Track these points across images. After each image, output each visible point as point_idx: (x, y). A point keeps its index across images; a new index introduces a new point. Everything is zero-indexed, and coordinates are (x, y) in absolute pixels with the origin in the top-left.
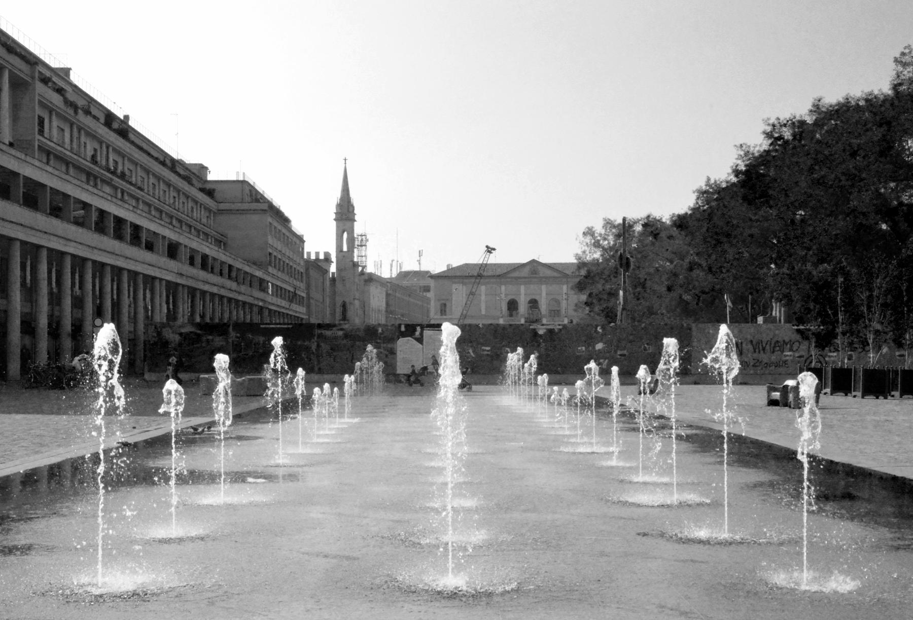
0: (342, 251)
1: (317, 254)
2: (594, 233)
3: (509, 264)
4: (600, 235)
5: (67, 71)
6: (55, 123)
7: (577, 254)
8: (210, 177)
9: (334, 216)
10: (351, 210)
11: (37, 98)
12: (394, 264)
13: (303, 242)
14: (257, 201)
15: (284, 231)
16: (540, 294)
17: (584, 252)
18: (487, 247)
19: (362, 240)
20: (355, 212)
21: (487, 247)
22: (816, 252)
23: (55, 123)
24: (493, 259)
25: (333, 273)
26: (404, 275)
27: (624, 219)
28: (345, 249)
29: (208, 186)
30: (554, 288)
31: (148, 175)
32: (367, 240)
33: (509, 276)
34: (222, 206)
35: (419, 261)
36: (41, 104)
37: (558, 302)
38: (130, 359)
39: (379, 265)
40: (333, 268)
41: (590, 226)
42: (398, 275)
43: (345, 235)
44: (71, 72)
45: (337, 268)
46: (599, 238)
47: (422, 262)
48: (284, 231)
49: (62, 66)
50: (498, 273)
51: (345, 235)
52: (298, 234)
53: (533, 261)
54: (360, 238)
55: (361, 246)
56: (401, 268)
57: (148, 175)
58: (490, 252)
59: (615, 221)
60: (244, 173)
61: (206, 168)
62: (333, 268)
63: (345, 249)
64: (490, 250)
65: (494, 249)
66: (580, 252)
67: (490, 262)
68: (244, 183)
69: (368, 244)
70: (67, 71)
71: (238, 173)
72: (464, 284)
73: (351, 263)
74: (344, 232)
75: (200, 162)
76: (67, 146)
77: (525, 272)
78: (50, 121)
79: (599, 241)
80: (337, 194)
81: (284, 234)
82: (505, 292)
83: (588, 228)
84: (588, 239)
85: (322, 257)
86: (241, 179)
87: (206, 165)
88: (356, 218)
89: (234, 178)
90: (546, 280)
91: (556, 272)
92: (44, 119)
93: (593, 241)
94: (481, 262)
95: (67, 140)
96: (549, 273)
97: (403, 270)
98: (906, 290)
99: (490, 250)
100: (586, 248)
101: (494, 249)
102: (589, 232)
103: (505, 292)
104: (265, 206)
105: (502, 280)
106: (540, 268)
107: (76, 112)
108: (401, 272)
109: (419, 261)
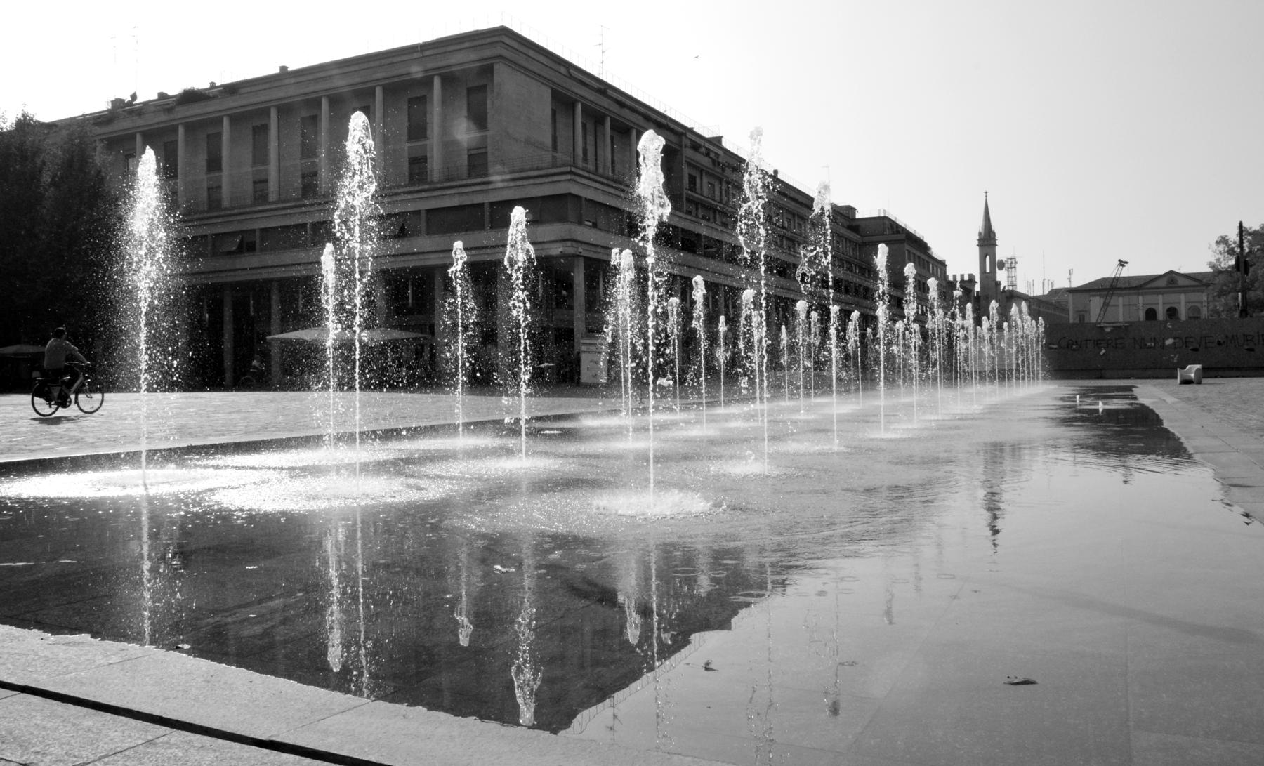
0: (985, 272)
1: (962, 276)
2: (1227, 241)
3: (1146, 276)
4: (1234, 242)
5: (719, 139)
6: (705, 180)
7: (1210, 263)
8: (858, 216)
9: (977, 242)
10: (992, 236)
11: (684, 159)
12: (1046, 282)
13: (945, 266)
14: (898, 232)
15: (923, 256)
16: (1179, 303)
17: (1218, 260)
18: (1120, 261)
19: (1012, 263)
20: (996, 238)
21: (1120, 261)
22: (447, 348)
23: (705, 180)
24: (1126, 272)
25: (978, 292)
26: (1055, 292)
27: (1242, 230)
28: (988, 270)
29: (854, 224)
30: (1194, 297)
31: (794, 217)
32: (1016, 263)
33: (1149, 286)
34: (866, 239)
35: (1070, 279)
36: (689, 164)
37: (1198, 310)
38: (361, 471)
39: (1031, 284)
40: (977, 288)
41: (1223, 234)
42: (1050, 292)
43: (988, 258)
44: (723, 139)
45: (981, 288)
46: (1233, 246)
47: (1072, 280)
48: (923, 256)
49: (715, 135)
50: (1134, 285)
51: (988, 258)
52: (940, 259)
53: (1171, 272)
54: (1010, 261)
55: (1011, 268)
56: (1052, 286)
57: (794, 217)
58: (1123, 266)
59: (1251, 228)
60: (884, 211)
61: (854, 209)
62: (977, 288)
63: (988, 270)
64: (1122, 264)
65: (1127, 263)
66: (1213, 260)
67: (1122, 275)
68: (885, 218)
69: (1017, 266)
70: (719, 139)
71: (879, 210)
72: (1100, 296)
73: (994, 284)
74: (986, 256)
75: (847, 204)
76: (717, 198)
77: (1162, 283)
78: (701, 179)
79: (1233, 248)
80: (979, 224)
81: (924, 260)
82: (1142, 302)
83: (1221, 237)
84: (1222, 247)
85: (966, 278)
86: (882, 215)
87: (853, 206)
88: (998, 243)
89: (877, 215)
90: (1184, 289)
91: (1197, 282)
92: (695, 177)
93: (1226, 249)
94: (1113, 276)
95: (717, 193)
96: (1187, 282)
97: (1055, 288)
98: (503, 566)
99: (1122, 264)
100: (1220, 256)
101: (1127, 263)
102: (1223, 240)
103: (1142, 302)
104: (903, 236)
105: (1140, 291)
106: (1176, 277)
107: (723, 170)
108: (1052, 290)
109: (1070, 279)
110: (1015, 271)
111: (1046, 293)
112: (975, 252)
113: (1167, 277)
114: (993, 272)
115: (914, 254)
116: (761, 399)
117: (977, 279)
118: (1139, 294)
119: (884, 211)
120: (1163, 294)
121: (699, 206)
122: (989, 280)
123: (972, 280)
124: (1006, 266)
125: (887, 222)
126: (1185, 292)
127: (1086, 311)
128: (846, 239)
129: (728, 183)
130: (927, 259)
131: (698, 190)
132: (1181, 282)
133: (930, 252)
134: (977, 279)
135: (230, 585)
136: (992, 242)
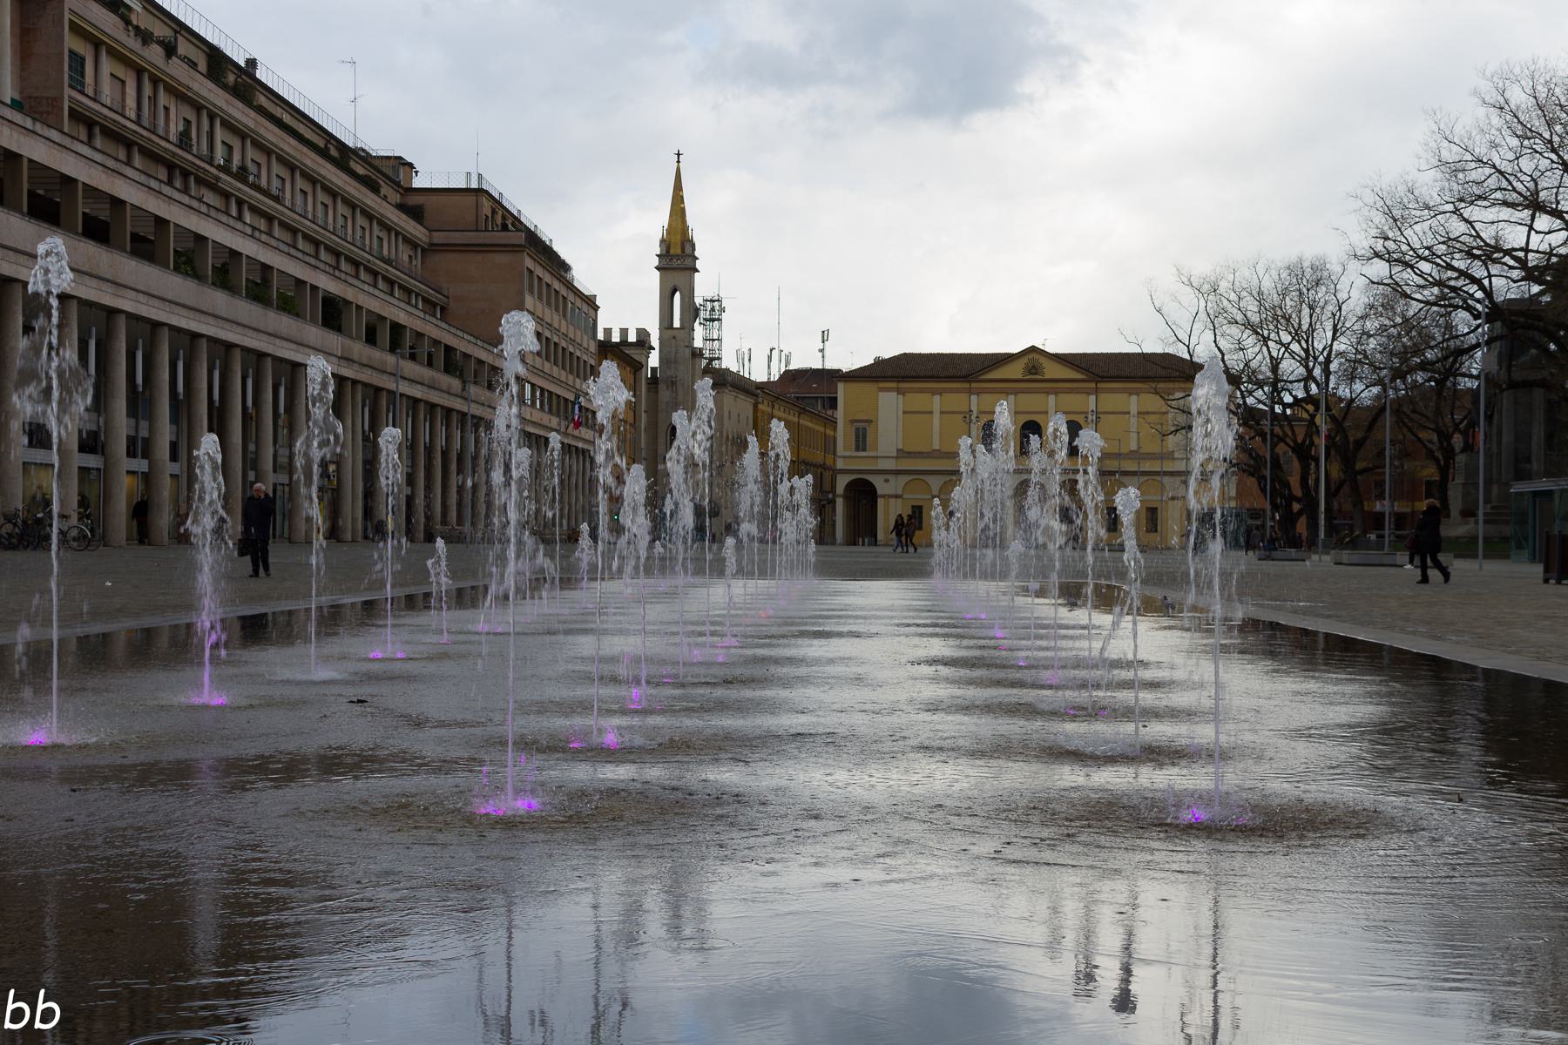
1: (624, 332)
6: (107, 66)
8: (417, 183)
9: (656, 261)
10: (688, 250)
11: (67, 16)
13: (596, 308)
15: (556, 285)
19: (713, 309)
25: (654, 370)
28: (677, 324)
29: (413, 200)
32: (723, 310)
36: (75, 28)
39: (746, 357)
40: (654, 360)
42: (782, 377)
48: (556, 285)
51: (677, 296)
53: (1033, 349)
55: (713, 320)
60: (480, 176)
62: (654, 360)
63: (677, 324)
68: (480, 192)
69: (724, 316)
71: (469, 174)
73: (688, 352)
77: (1015, 371)
80: (657, 222)
85: (632, 338)
86: (474, 185)
88: (698, 265)
90: (1055, 386)
92: (83, 59)
95: (131, 102)
97: (792, 367)
104: (520, 238)
110: (720, 326)
111: (775, 377)
112: (653, 281)
113: (1024, 360)
114: (688, 327)
115: (540, 279)
116: (863, 545)
117: (655, 342)
118: (970, 392)
119: (480, 176)
120: (1056, 394)
121: (97, 130)
122: (676, 339)
123: (643, 342)
124: (702, 314)
125: (486, 207)
126: (1056, 392)
127: (869, 421)
128: (397, 233)
129: (155, 81)
130: (563, 291)
131: (89, 91)
132: (1052, 371)
133: (568, 276)
134: (655, 342)
135: (99, 840)
136: (688, 262)
